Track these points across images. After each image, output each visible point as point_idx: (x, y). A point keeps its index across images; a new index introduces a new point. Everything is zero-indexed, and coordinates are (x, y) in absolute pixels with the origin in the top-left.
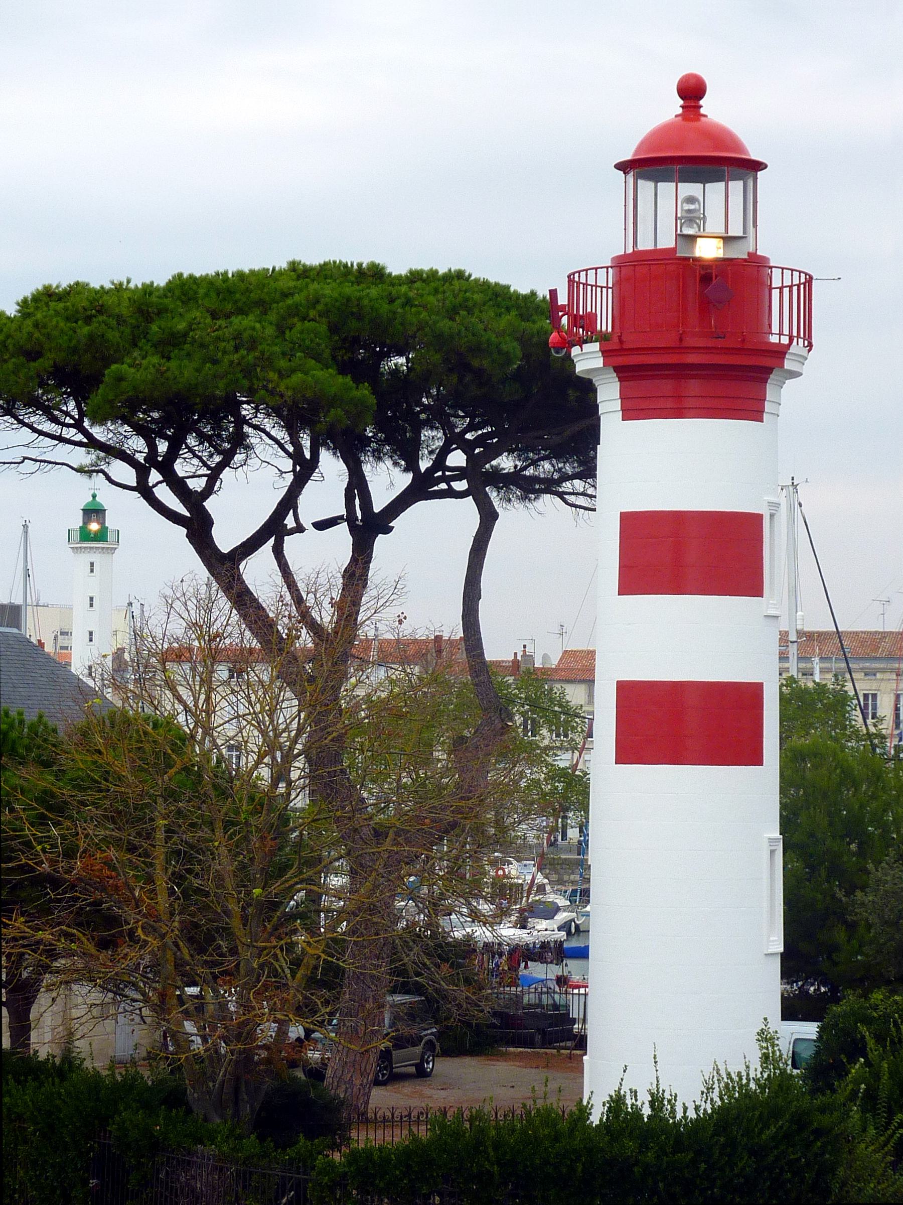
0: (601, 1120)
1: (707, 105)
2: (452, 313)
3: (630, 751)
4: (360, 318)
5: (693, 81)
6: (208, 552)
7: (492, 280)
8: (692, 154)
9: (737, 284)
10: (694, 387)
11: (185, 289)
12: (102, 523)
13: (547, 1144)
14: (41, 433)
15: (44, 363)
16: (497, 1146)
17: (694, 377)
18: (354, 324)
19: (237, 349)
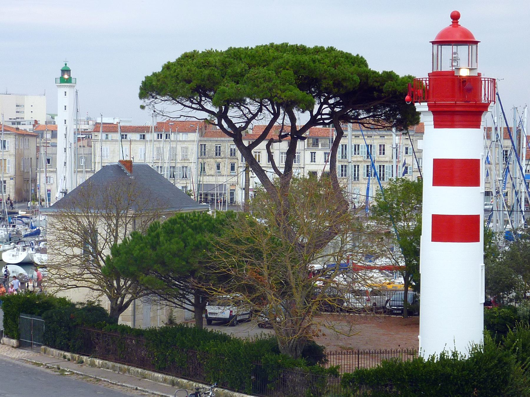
0: (428, 360)
1: (460, 21)
2: (335, 66)
3: (437, 237)
4: (304, 68)
5: (456, 14)
6: (241, 147)
7: (345, 51)
8: (455, 36)
9: (472, 84)
10: (457, 118)
11: (235, 54)
12: (69, 75)
13: (422, 369)
14: (185, 106)
15: (193, 84)
16: (406, 369)
17: (457, 115)
18: (302, 71)
19: (265, 81)
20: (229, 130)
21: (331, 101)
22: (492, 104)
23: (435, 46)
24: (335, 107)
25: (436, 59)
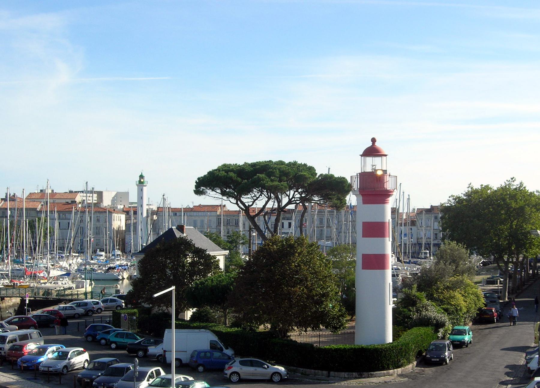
20: (243, 207)
21: (300, 190)
22: (395, 190)
23: (363, 158)
24: (302, 194)
25: (364, 164)
